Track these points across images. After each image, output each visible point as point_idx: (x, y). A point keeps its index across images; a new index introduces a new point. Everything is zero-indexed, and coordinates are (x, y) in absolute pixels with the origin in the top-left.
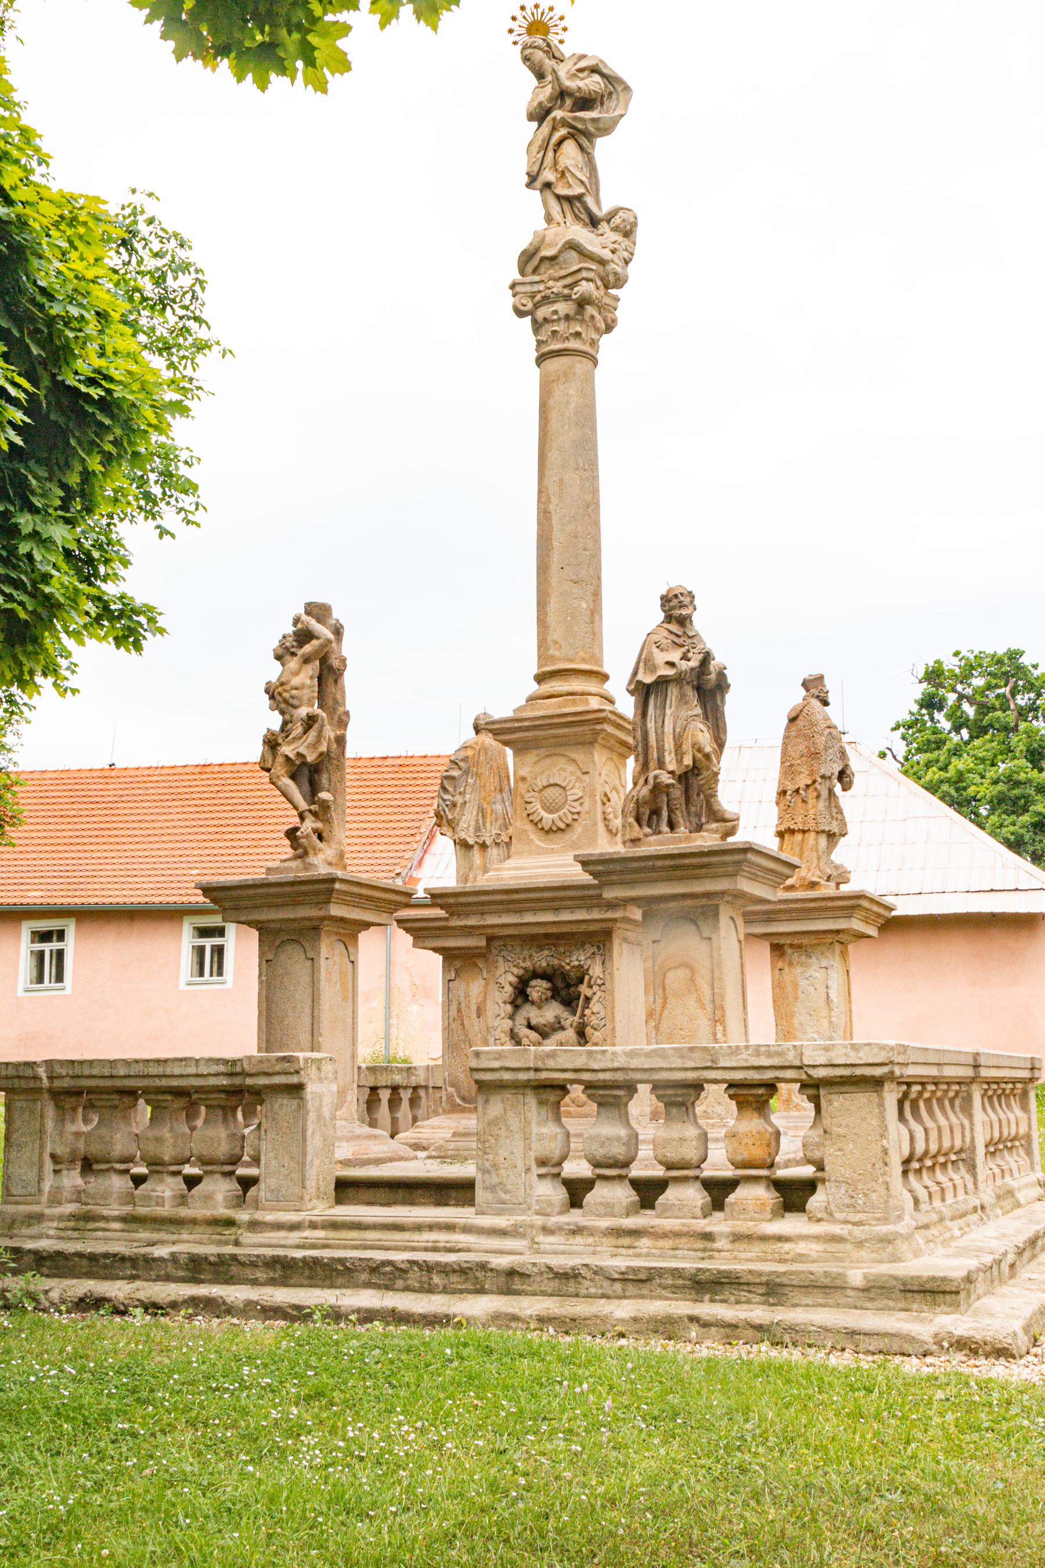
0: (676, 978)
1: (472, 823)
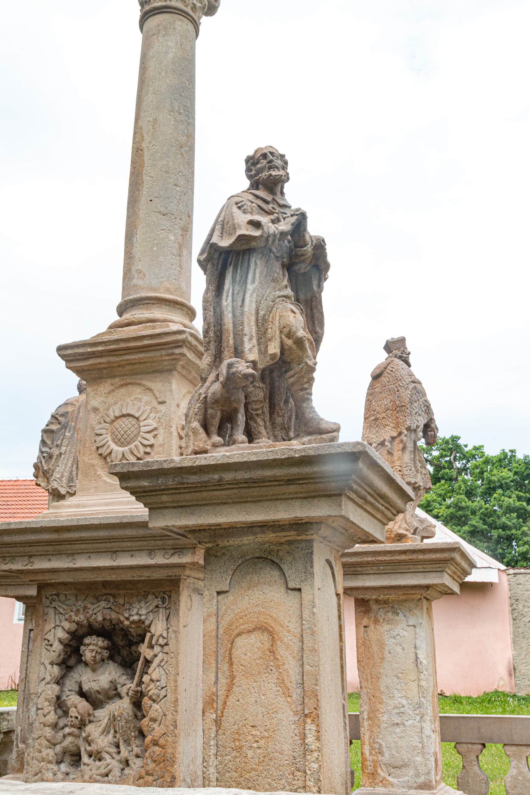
0: (248, 647)
1: (66, 474)
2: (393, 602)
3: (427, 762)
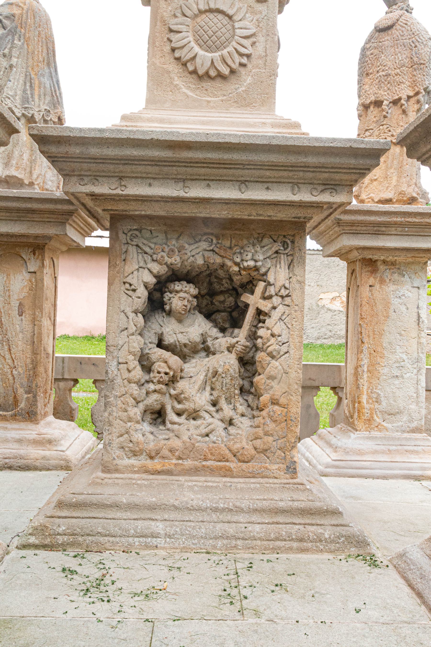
2: (400, 263)
3: (421, 409)
